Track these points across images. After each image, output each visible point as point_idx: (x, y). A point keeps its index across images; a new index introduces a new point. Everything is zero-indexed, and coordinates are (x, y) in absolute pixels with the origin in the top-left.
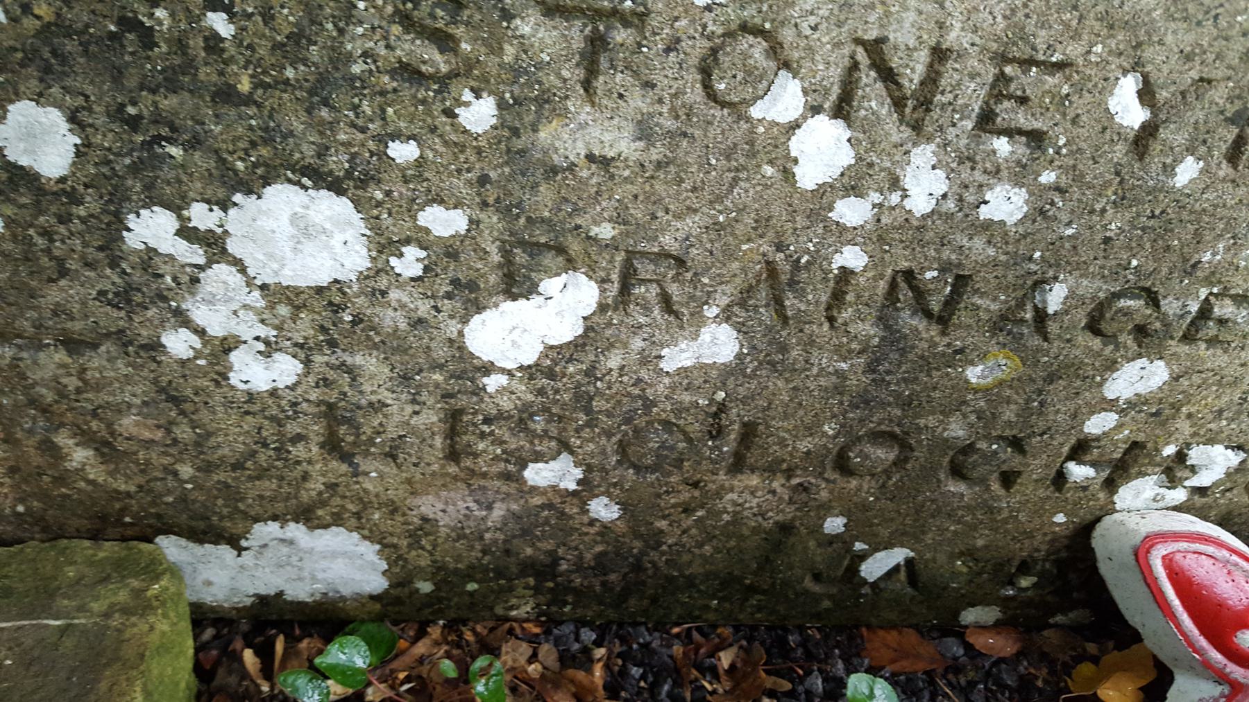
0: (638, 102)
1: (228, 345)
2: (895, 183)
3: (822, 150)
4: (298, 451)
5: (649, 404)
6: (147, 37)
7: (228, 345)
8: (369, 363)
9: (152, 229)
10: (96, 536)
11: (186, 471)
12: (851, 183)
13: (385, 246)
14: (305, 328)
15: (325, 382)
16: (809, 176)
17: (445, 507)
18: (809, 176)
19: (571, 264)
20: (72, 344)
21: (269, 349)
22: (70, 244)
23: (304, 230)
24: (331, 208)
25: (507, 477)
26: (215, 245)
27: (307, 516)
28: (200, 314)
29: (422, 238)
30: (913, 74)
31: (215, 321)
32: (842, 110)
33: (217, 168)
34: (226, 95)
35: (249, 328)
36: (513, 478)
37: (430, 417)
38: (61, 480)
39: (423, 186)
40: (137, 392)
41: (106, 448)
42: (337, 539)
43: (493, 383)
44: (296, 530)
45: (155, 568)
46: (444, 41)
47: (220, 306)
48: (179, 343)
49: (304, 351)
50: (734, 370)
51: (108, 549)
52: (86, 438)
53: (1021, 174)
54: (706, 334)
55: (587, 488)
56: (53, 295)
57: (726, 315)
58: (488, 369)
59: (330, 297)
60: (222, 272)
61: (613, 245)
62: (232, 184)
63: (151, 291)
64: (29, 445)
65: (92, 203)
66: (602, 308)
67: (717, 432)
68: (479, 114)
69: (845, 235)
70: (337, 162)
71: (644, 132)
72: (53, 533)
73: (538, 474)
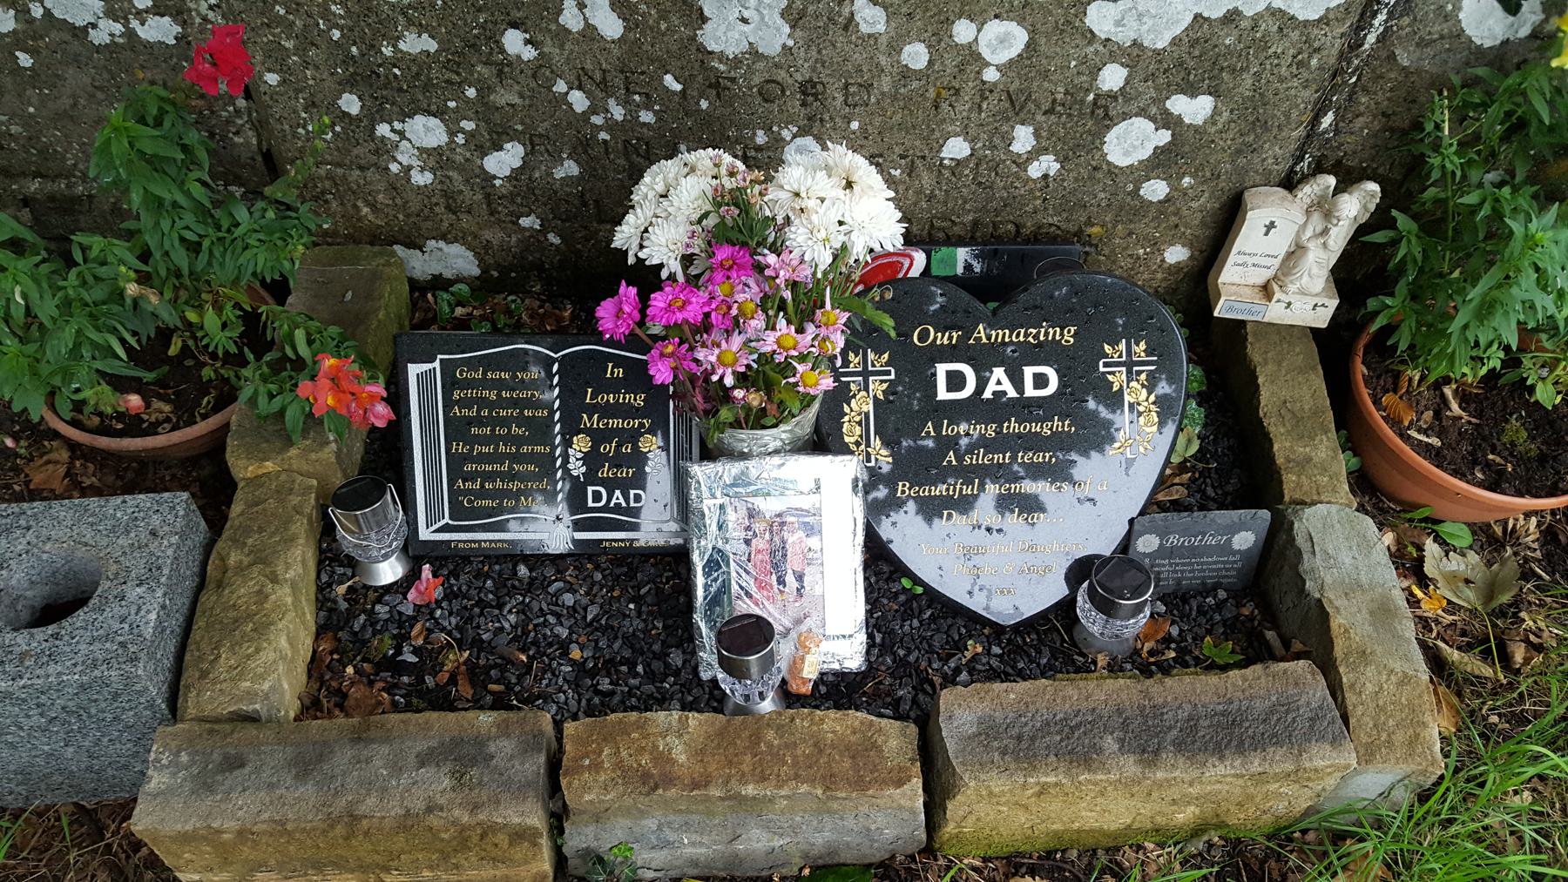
0: (517, 87)
1: (410, 168)
2: (607, 111)
3: (579, 101)
4: (437, 209)
5: (555, 192)
6: (378, 76)
7: (410, 168)
8: (454, 174)
9: (383, 130)
10: (372, 244)
11: (401, 217)
12: (593, 110)
13: (452, 134)
14: (432, 163)
15: (441, 182)
16: (579, 108)
17: (493, 236)
18: (579, 108)
19: (512, 140)
20: (361, 168)
21: (422, 170)
22: (360, 135)
23: (427, 129)
24: (434, 122)
25: (513, 223)
26: (401, 134)
27: (444, 237)
28: (399, 157)
29: (462, 131)
30: (598, 76)
31: (404, 159)
32: (580, 88)
33: (596, 767)
34: (400, 90)
35: (416, 163)
36: (516, 223)
37: (479, 197)
38: (359, 220)
39: (460, 114)
40: (381, 186)
41: (373, 206)
42: (456, 249)
43: (498, 183)
44: (442, 244)
45: (394, 254)
46: (458, 74)
47: (406, 155)
48: (394, 168)
49: (433, 170)
50: (581, 177)
51: (376, 248)
52: (368, 204)
53: (648, 107)
54: (566, 164)
55: (544, 229)
56: (355, 151)
57: (570, 157)
58: (495, 177)
59: (438, 151)
60: (404, 142)
61: (522, 132)
62: (405, 116)
63: (384, 150)
64: (349, 206)
65: (365, 122)
66: (526, 154)
67: (585, 204)
68: (471, 93)
69: (599, 128)
70: (434, 108)
71: (521, 96)
72: (357, 242)
73: (525, 222)
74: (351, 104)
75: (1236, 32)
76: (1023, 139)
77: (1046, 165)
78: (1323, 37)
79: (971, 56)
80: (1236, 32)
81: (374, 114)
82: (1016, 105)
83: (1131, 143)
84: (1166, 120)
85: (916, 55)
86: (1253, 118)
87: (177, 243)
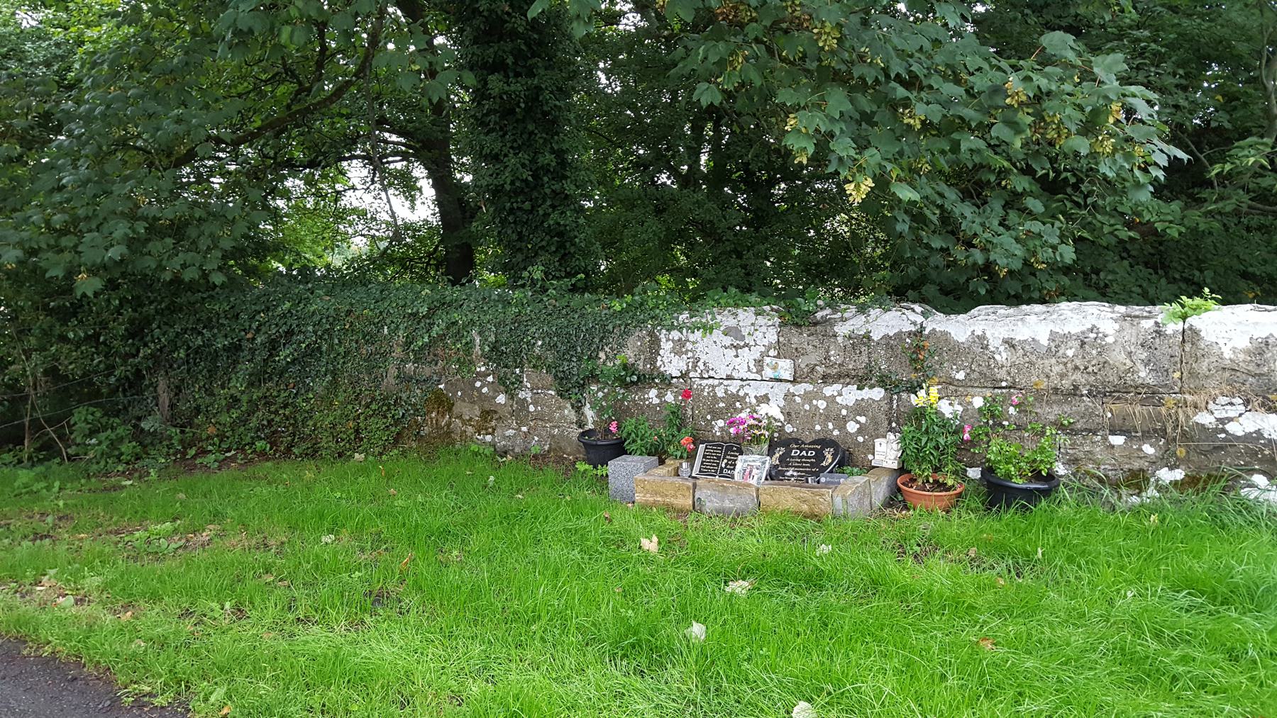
63: (713, 427)
74: (709, 417)
75: (982, 644)
76: (831, 426)
77: (836, 433)
78: (883, 404)
79: (817, 407)
80: (982, 644)
81: (712, 419)
82: (828, 418)
83: (852, 427)
84: (858, 422)
85: (807, 407)
86: (874, 421)
87: (893, 53)
